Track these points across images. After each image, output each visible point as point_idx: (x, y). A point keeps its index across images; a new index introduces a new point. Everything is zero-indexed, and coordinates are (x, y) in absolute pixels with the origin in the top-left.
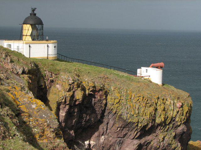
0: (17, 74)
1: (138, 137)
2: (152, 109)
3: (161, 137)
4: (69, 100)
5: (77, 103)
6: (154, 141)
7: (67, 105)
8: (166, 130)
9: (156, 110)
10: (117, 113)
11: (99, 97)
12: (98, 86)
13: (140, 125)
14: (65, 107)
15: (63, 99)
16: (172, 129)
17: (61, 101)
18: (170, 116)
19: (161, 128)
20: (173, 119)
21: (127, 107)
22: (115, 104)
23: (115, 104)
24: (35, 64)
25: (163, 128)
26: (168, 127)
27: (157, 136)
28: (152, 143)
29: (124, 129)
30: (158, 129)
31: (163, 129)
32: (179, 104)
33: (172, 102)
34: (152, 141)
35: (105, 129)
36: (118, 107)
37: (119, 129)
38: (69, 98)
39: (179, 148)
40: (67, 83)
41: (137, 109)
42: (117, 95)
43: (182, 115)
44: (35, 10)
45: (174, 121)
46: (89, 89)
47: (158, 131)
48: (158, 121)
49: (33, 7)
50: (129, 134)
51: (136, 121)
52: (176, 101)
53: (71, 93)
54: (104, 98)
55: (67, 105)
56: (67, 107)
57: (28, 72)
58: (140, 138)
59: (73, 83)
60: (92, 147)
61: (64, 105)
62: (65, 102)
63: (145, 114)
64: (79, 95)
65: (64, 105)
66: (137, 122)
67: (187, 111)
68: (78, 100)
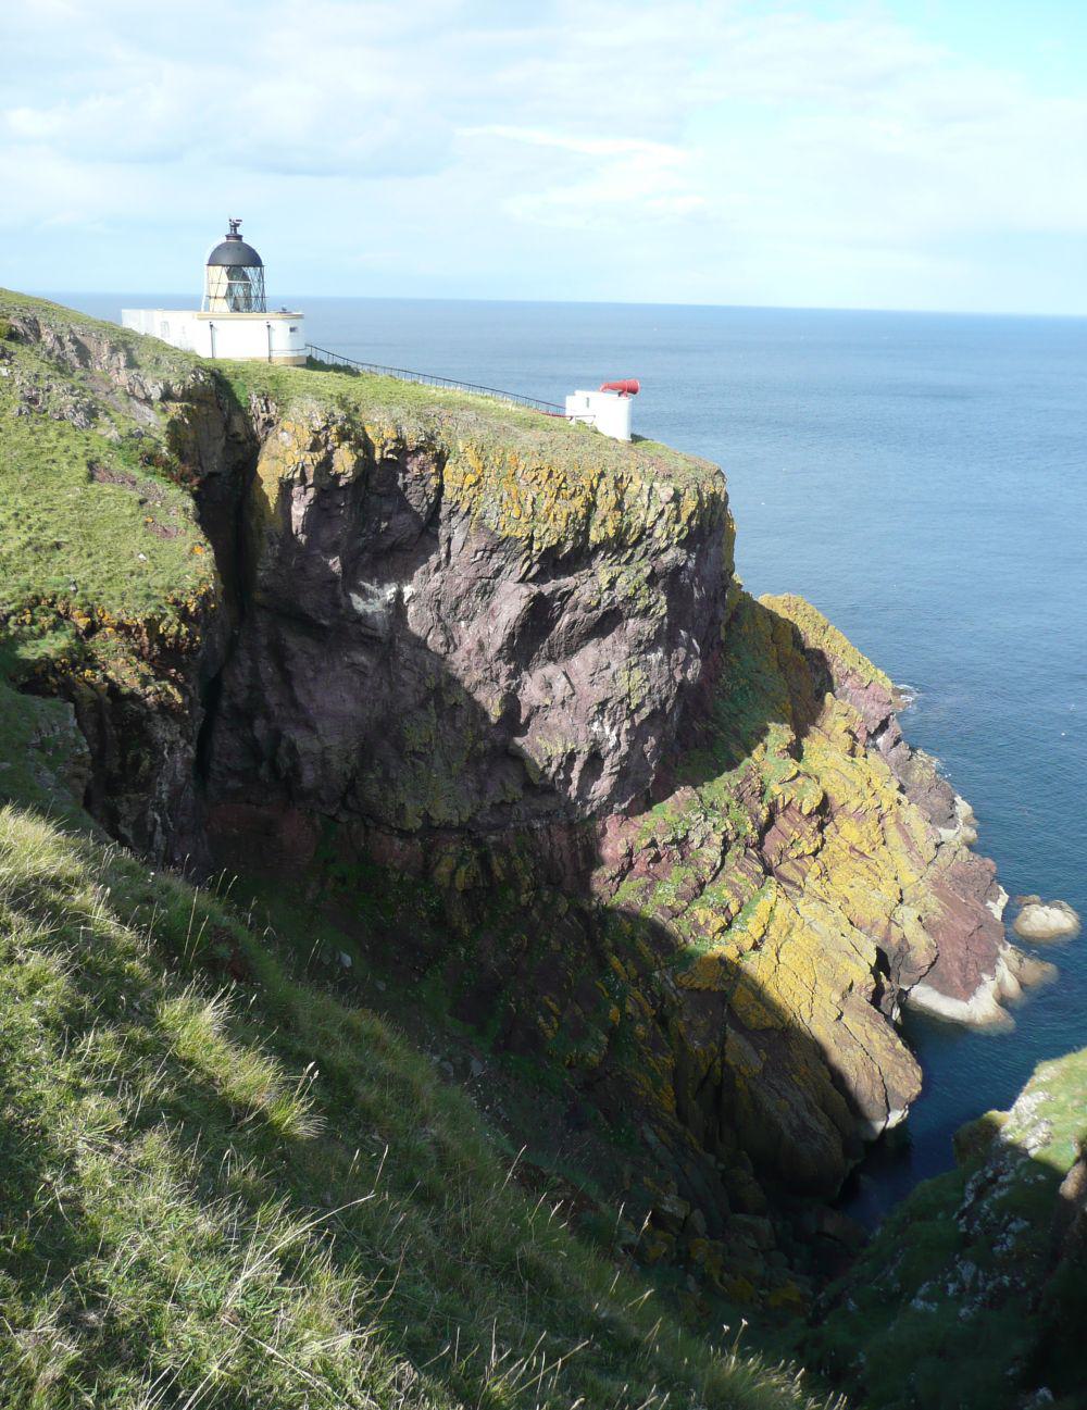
0: (148, 400)
1: (534, 576)
2: (578, 502)
3: (603, 578)
4: (312, 473)
5: (342, 483)
6: (582, 588)
7: (310, 486)
8: (623, 560)
9: (591, 506)
10: (473, 511)
11: (416, 469)
12: (413, 434)
13: (536, 546)
14: (305, 493)
15: (296, 470)
16: (643, 557)
17: (290, 476)
18: (637, 524)
19: (605, 554)
20: (647, 532)
21: (498, 497)
22: (466, 487)
23: (466, 487)
24: (213, 374)
25: (611, 557)
26: (630, 551)
27: (593, 575)
28: (577, 593)
29: (494, 556)
30: (599, 558)
31: (614, 558)
32: (665, 492)
33: (646, 487)
34: (576, 587)
35: (444, 555)
36: (474, 496)
37: (479, 554)
38: (312, 469)
39: (661, 608)
40: (306, 428)
41: (529, 503)
42: (473, 462)
43: (677, 521)
44: (238, 225)
45: (650, 536)
46: (383, 447)
47: (597, 563)
48: (595, 536)
49: (234, 219)
50: (508, 568)
51: (525, 535)
52: (656, 485)
53: (320, 456)
54: (433, 470)
55: (310, 486)
56: (311, 492)
57: (182, 396)
58: (540, 578)
59: (326, 428)
60: (408, 601)
61: (302, 488)
62: (303, 478)
63: (555, 515)
64: (345, 461)
65: (302, 488)
66: (527, 538)
67: (693, 513)
68: (344, 473)
